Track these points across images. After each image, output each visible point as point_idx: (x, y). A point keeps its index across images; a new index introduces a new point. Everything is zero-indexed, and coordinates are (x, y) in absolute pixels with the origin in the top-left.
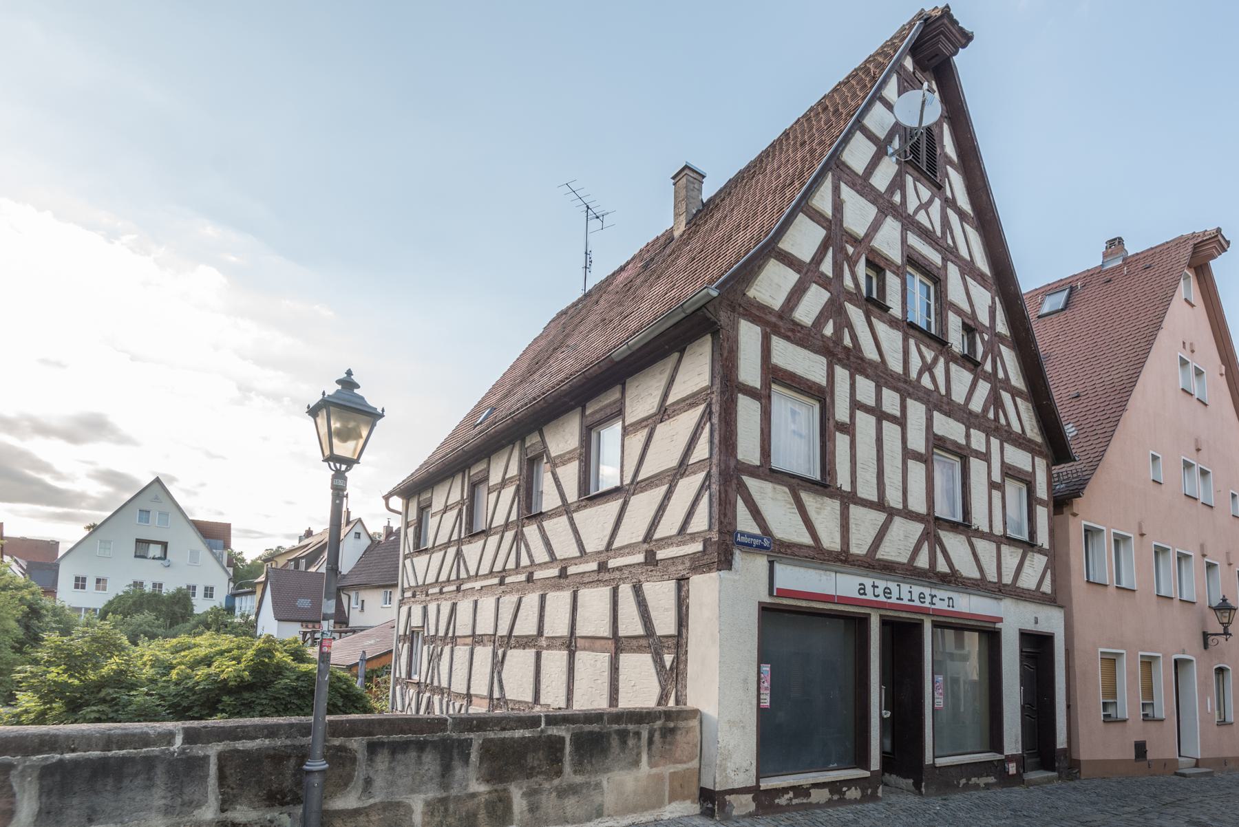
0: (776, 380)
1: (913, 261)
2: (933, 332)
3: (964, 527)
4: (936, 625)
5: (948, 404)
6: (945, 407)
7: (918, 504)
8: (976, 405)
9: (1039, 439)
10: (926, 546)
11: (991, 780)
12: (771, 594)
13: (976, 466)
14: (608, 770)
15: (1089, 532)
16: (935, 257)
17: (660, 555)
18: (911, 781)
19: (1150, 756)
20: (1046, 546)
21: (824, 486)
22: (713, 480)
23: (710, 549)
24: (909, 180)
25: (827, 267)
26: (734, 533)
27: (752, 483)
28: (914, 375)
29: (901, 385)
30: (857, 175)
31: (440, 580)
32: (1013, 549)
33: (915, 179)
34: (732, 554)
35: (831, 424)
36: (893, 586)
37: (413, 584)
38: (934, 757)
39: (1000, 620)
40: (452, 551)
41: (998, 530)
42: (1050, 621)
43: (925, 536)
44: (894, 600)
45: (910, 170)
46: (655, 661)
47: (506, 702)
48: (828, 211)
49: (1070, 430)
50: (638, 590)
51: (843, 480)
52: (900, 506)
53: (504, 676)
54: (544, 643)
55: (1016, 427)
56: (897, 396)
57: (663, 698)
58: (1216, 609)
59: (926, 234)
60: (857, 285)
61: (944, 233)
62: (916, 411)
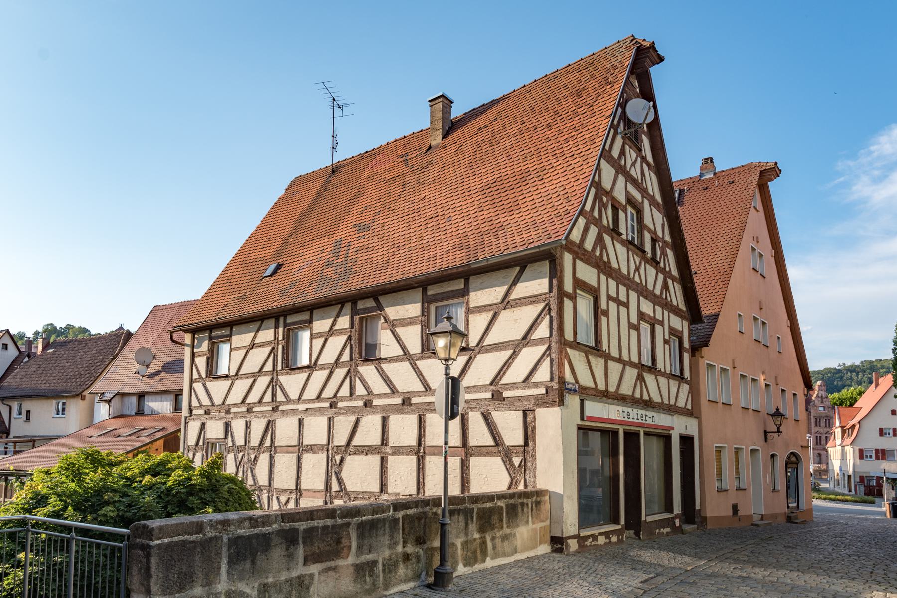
1: (630, 201)
4: (646, 434)
7: (635, 359)
8: (588, 245)
9: (684, 309)
11: (668, 530)
12: (582, 418)
13: (658, 328)
14: (518, 526)
18: (632, 532)
19: (740, 513)
22: (553, 351)
23: (551, 393)
25: (596, 214)
33: (630, 147)
42: (680, 426)
44: (631, 420)
47: (347, 494)
50: (487, 417)
53: (344, 474)
58: (773, 415)
59: (634, 182)
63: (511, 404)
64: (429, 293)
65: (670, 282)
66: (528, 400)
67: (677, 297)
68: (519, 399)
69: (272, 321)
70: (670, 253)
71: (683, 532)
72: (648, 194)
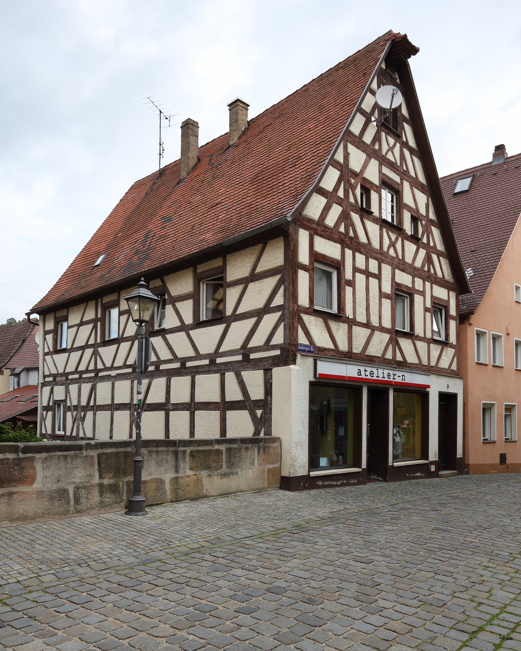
0: (317, 261)
1: (386, 183)
2: (395, 223)
3: (410, 335)
5: (403, 265)
6: (402, 266)
7: (387, 323)
8: (418, 264)
9: (452, 280)
10: (391, 347)
13: (418, 298)
15: (480, 335)
16: (396, 178)
17: (253, 356)
19: (508, 462)
20: (454, 343)
21: (339, 317)
24: (383, 134)
25: (341, 193)
26: (297, 345)
27: (306, 318)
28: (385, 249)
29: (378, 256)
30: (355, 136)
31: (80, 369)
32: (436, 346)
33: (386, 134)
34: (296, 356)
35: (343, 282)
36: (375, 370)
37: (54, 371)
38: (393, 462)
39: (429, 386)
40: (89, 352)
41: (429, 335)
42: (455, 386)
43: (390, 341)
44: (375, 378)
45: (383, 129)
46: (250, 414)
48: (342, 161)
49: (469, 272)
51: (349, 313)
52: (378, 325)
54: (171, 407)
55: (440, 274)
56: (376, 262)
57: (257, 432)
59: (392, 166)
60: (356, 201)
61: (401, 163)
62: (386, 269)
63: (256, 364)
64: (199, 271)
65: (434, 257)
66: (267, 361)
67: (442, 268)
68: (261, 360)
69: (93, 302)
70: (436, 232)
71: (438, 476)
72: (410, 177)
